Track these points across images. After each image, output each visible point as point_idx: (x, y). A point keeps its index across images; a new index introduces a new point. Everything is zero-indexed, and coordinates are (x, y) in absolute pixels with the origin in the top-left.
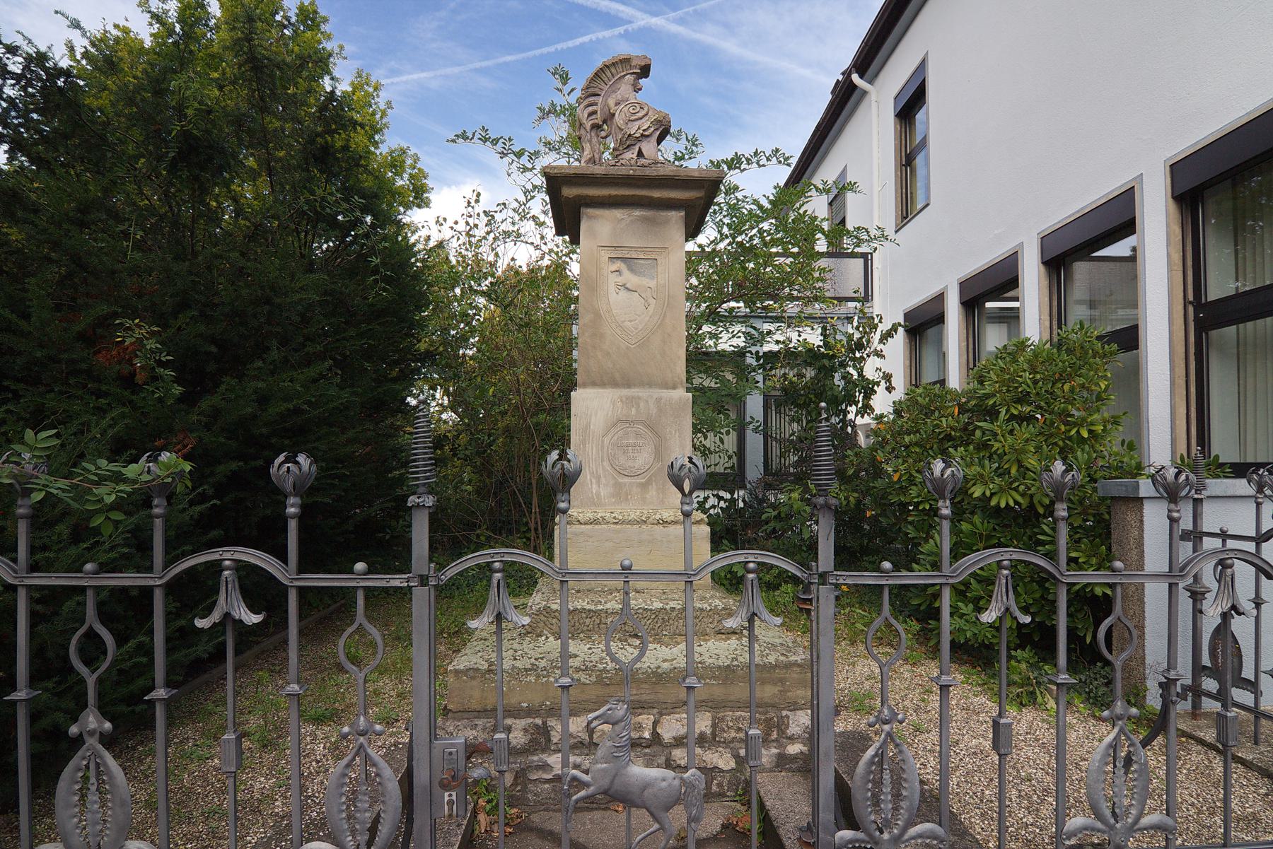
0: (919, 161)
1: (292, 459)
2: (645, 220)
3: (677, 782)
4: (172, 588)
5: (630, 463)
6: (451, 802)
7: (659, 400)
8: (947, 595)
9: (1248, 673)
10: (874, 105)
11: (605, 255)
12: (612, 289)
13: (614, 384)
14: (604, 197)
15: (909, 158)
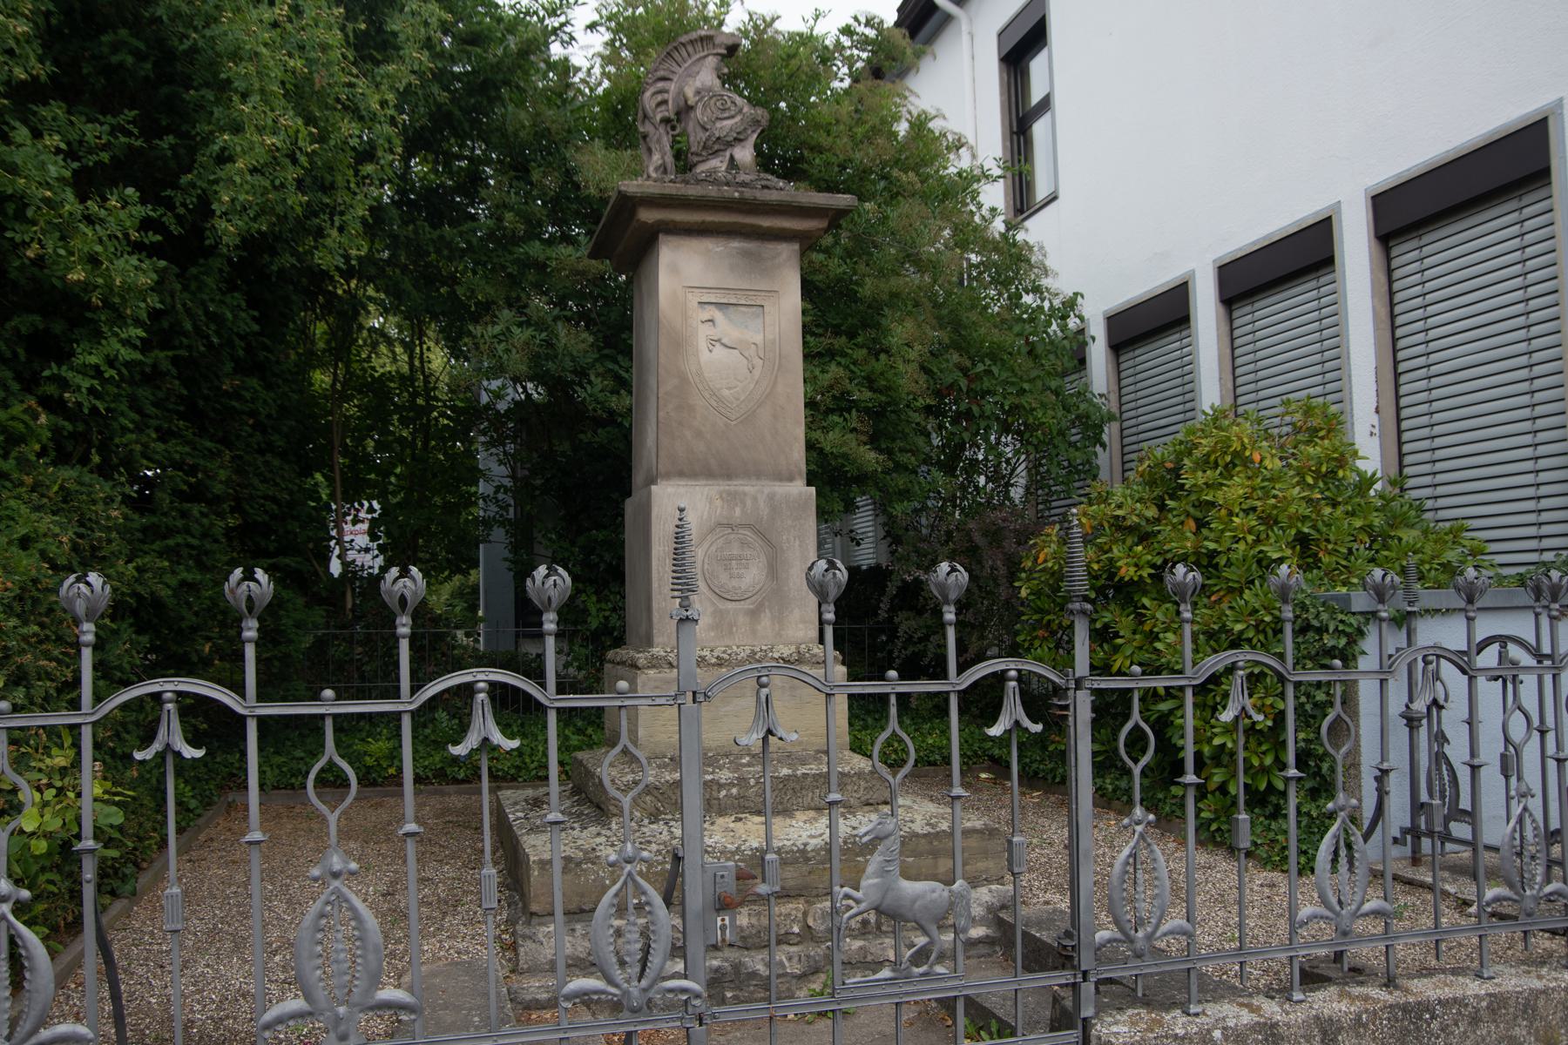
0: (1039, 129)
1: (82, 579)
2: (746, 254)
3: (946, 894)
4: (422, 716)
5: (735, 583)
6: (723, 928)
7: (771, 497)
8: (1189, 693)
9: (1465, 804)
10: (965, 38)
11: (694, 299)
12: (703, 344)
15: (1021, 119)
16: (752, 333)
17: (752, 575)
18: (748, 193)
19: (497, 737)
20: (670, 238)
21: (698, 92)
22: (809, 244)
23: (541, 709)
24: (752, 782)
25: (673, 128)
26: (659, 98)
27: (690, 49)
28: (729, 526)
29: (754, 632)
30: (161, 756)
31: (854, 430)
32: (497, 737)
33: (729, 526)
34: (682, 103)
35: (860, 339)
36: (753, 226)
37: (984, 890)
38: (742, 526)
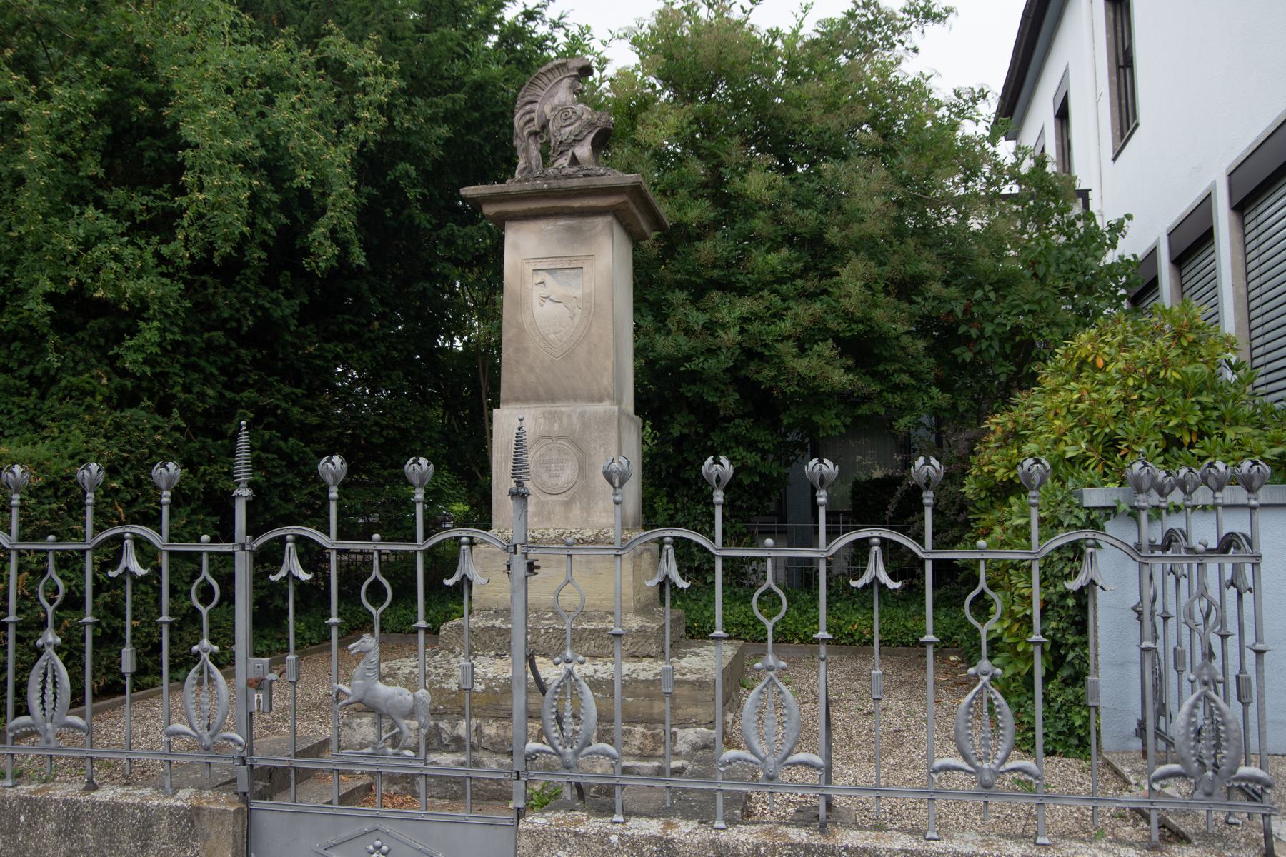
1: (716, 462)
2: (569, 229)
5: (553, 481)
7: (582, 415)
11: (529, 267)
12: (536, 301)
13: (538, 398)
16: (574, 288)
17: (567, 475)
18: (554, 183)
19: (884, 578)
21: (553, 110)
22: (618, 214)
23: (922, 562)
24: (542, 632)
25: (542, 138)
26: (528, 117)
27: (550, 76)
28: (550, 437)
29: (567, 518)
30: (286, 579)
32: (884, 578)
33: (550, 437)
37: (691, 731)
38: (564, 437)
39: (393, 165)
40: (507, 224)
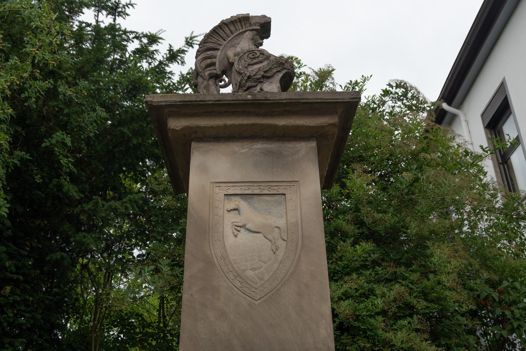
2: (268, 153)
10: (464, 124)
11: (220, 192)
12: (228, 231)
14: (219, 127)
16: (276, 217)
20: (201, 145)
26: (209, 61)
27: (232, 28)
31: (417, 330)
34: (226, 63)
35: (414, 267)
36: (270, 126)
39: (49, 135)
40: (193, 144)
